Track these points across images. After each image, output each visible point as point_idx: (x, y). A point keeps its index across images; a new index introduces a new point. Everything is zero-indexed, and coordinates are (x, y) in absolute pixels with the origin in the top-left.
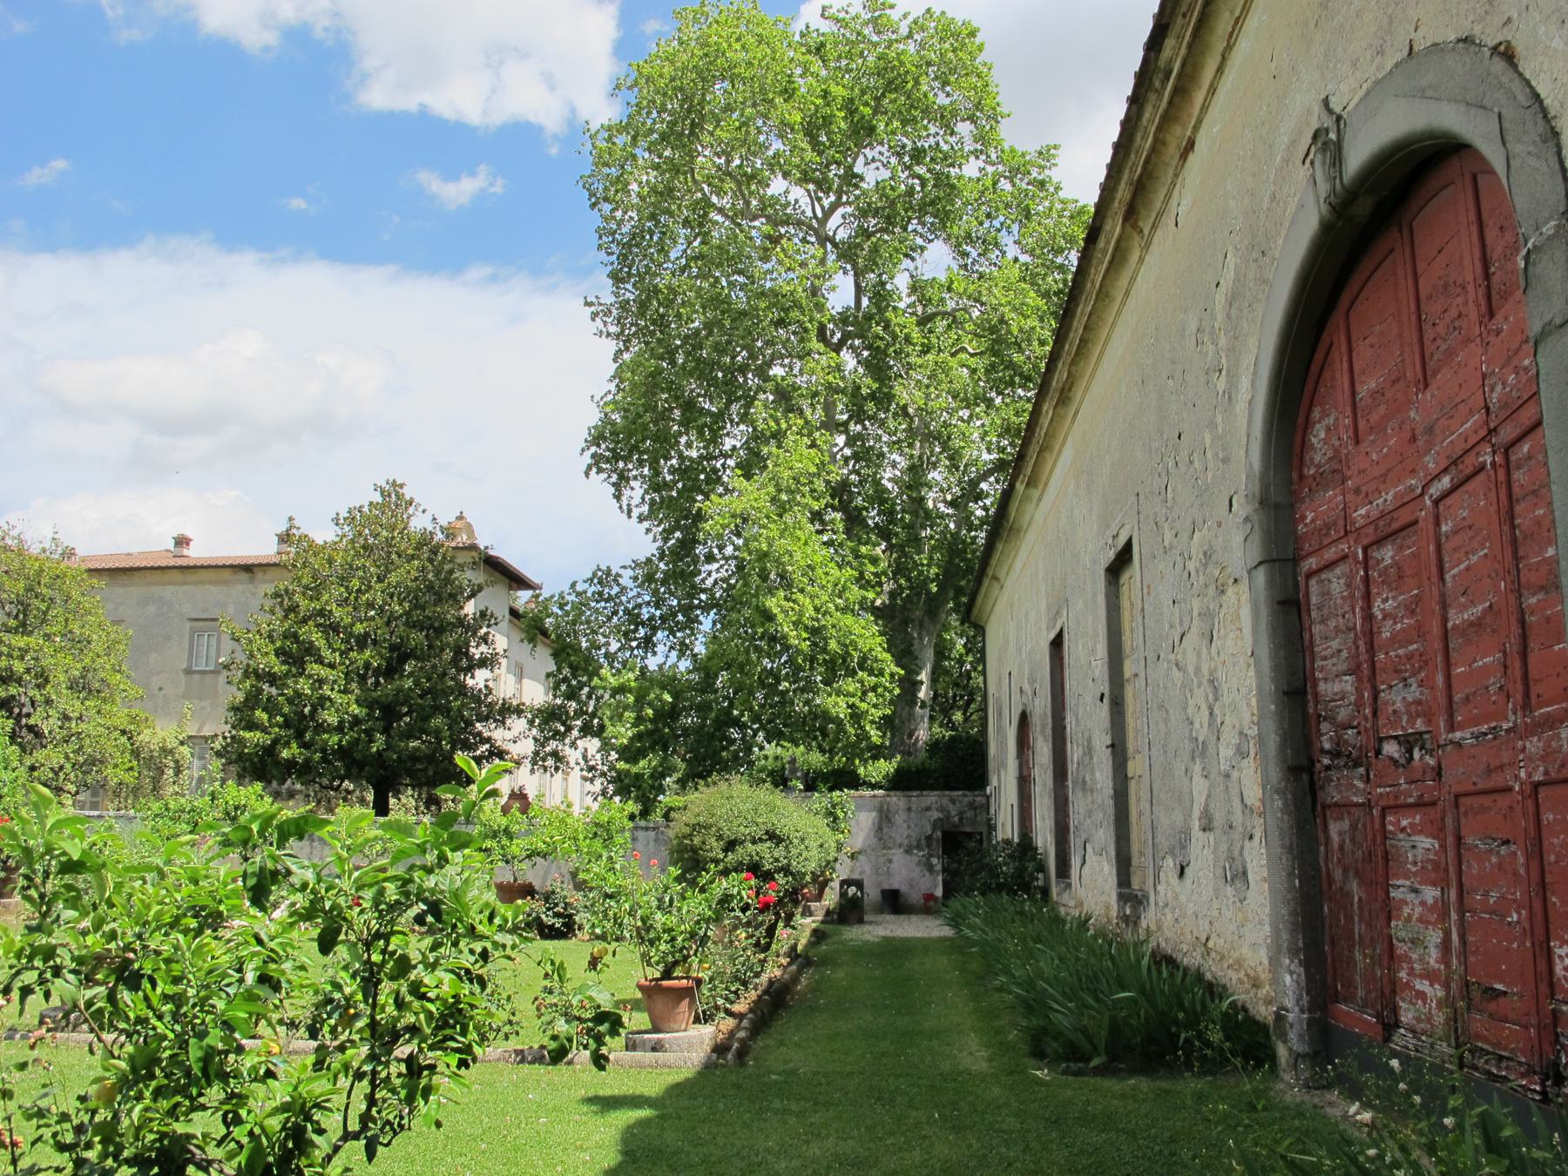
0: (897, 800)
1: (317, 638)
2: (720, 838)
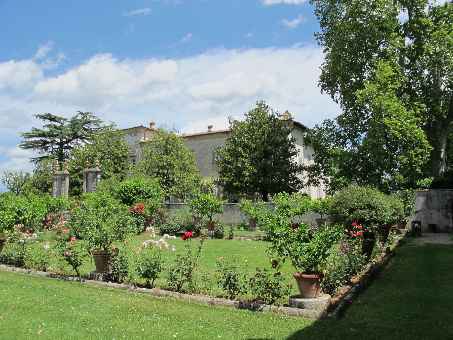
0: (433, 193)
1: (241, 150)
2: (347, 208)
